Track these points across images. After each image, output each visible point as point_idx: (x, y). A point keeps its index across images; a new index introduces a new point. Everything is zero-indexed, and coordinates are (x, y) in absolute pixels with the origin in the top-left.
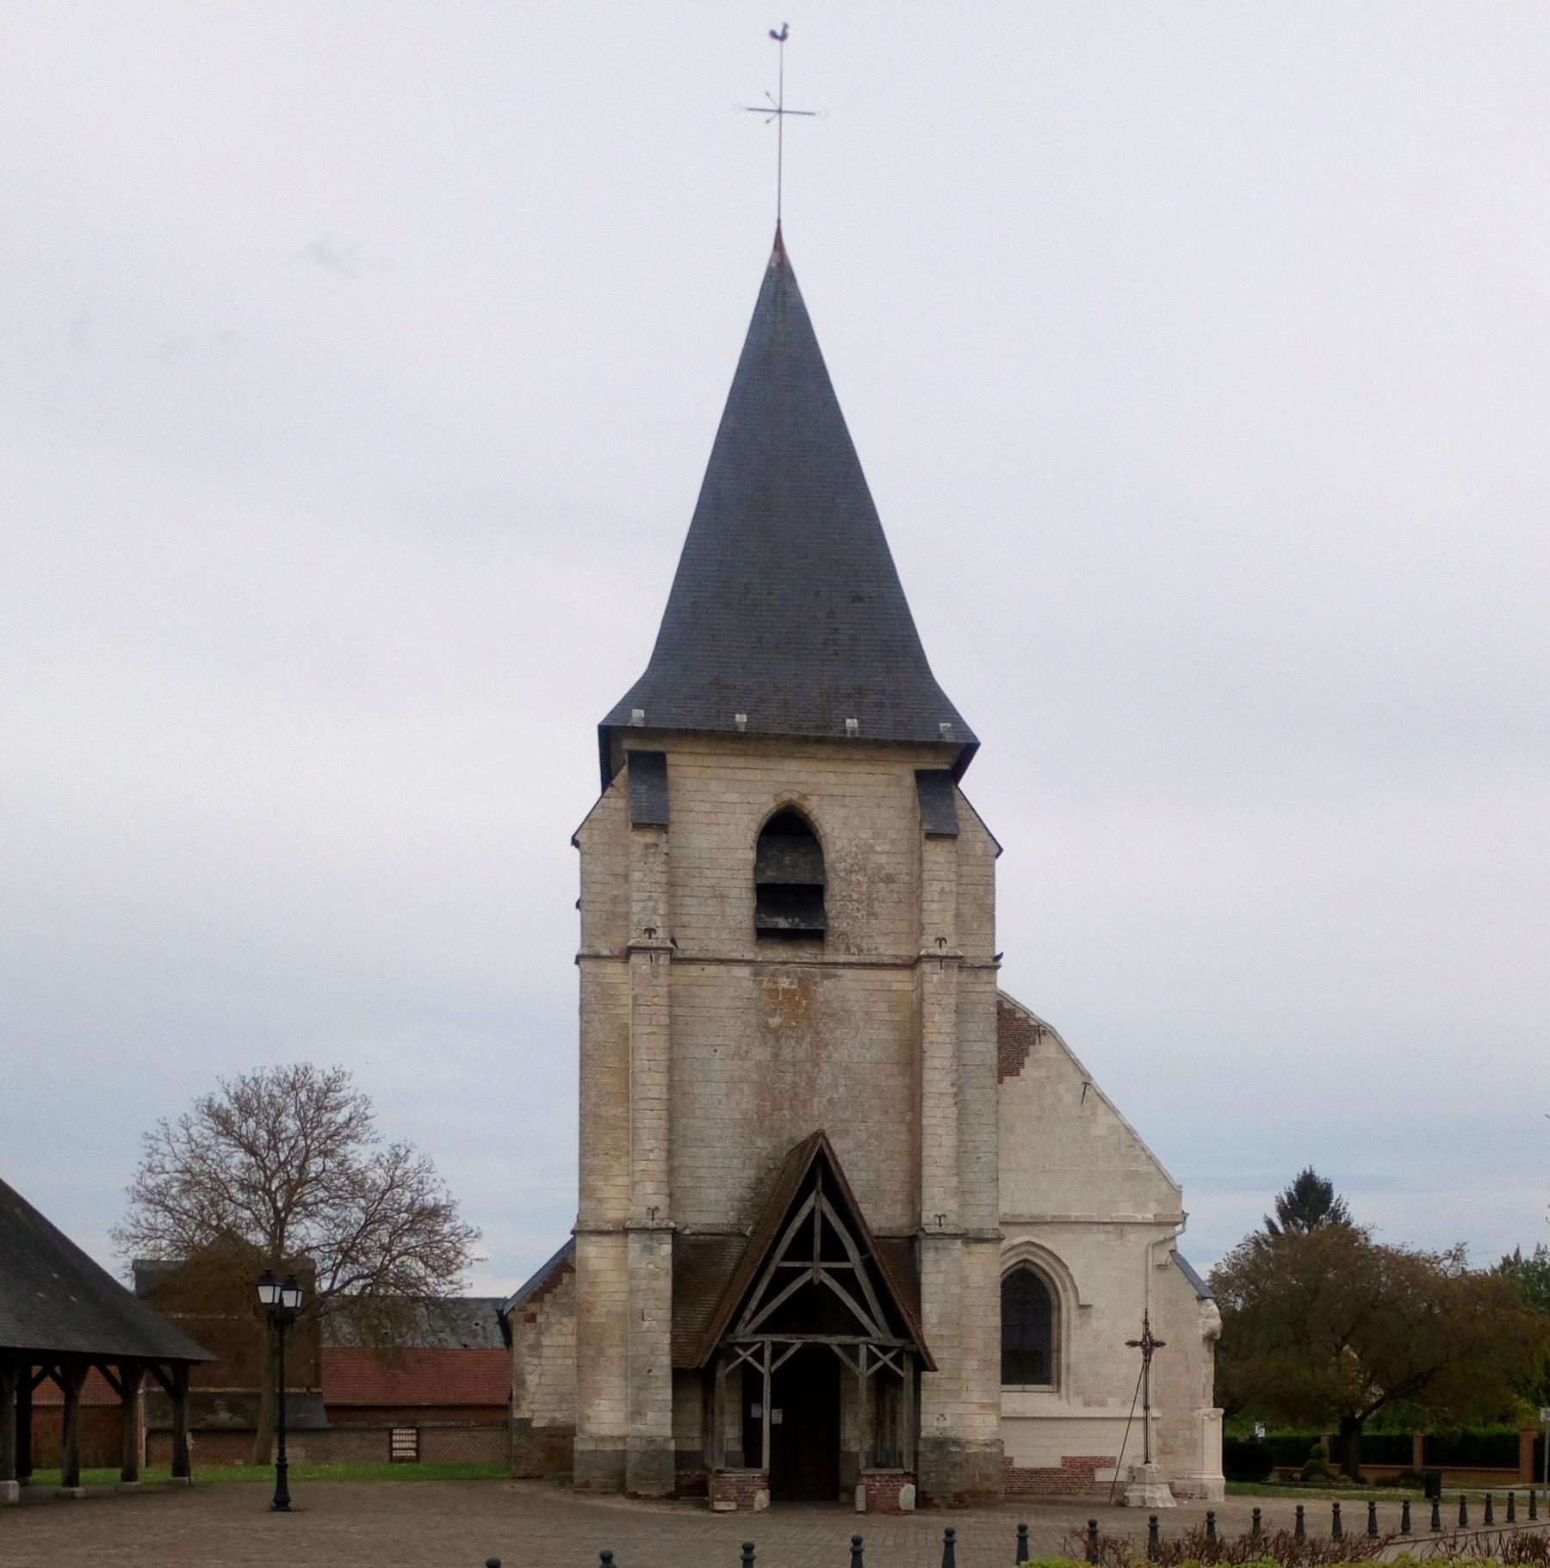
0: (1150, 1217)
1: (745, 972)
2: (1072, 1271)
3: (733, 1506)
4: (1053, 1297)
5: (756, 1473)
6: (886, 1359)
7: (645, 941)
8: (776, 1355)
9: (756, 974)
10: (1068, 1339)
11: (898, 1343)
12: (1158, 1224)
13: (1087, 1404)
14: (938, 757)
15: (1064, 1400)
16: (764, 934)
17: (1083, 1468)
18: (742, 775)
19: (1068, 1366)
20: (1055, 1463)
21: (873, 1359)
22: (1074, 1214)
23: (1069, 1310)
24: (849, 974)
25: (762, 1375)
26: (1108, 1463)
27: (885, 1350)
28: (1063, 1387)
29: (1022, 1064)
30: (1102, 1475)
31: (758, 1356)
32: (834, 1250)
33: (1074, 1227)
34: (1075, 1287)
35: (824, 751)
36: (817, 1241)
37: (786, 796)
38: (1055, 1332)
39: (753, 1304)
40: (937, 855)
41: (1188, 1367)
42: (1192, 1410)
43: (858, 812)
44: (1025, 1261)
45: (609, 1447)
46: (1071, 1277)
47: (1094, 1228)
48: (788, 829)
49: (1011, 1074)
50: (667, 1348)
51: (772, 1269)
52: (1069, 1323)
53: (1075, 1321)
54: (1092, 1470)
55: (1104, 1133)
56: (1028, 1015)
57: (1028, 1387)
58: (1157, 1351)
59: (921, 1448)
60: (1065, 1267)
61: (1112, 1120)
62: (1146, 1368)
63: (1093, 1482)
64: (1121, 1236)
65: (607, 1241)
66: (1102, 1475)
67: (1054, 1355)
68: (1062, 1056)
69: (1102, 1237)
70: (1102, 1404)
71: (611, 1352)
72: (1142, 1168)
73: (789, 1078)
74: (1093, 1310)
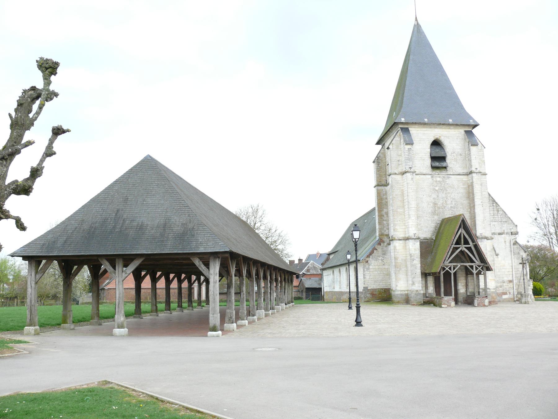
1: (430, 176)
3: (446, 306)
5: (451, 297)
6: (480, 268)
7: (409, 170)
8: (454, 269)
9: (432, 177)
11: (482, 264)
14: (469, 128)
16: (434, 168)
18: (426, 132)
21: (477, 268)
24: (453, 176)
25: (451, 273)
27: (479, 266)
31: (450, 269)
32: (466, 242)
35: (444, 127)
36: (462, 240)
37: (436, 137)
39: (448, 256)
40: (473, 149)
43: (453, 140)
45: (404, 293)
48: (436, 143)
50: (420, 268)
51: (452, 247)
59: (480, 291)
65: (401, 242)
71: (403, 269)
73: (441, 202)
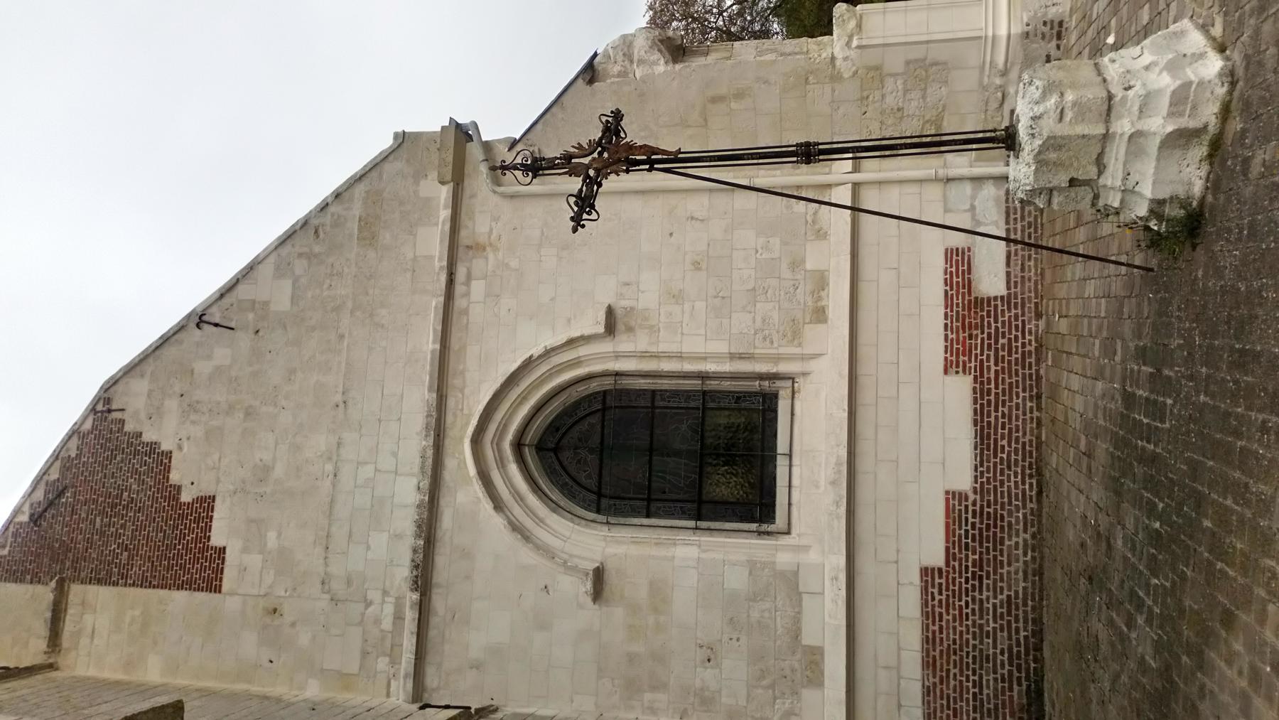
0: (444, 193)
2: (536, 351)
4: (594, 386)
10: (680, 357)
12: (458, 179)
13: (820, 315)
15: (812, 366)
17: (969, 316)
19: (733, 357)
20: (961, 388)
22: (430, 344)
23: (618, 356)
26: (959, 267)
28: (783, 368)
29: (153, 446)
30: (991, 278)
33: (454, 344)
34: (571, 343)
38: (665, 384)
41: (739, 95)
42: (836, 78)
44: (518, 446)
46: (548, 353)
47: (459, 303)
49: (168, 469)
52: (644, 355)
53: (642, 342)
54: (979, 303)
55: (287, 285)
56: (74, 432)
57: (782, 446)
58: (634, 133)
60: (528, 365)
61: (267, 269)
62: (673, 162)
63: (1007, 300)
64: (478, 248)
66: (991, 278)
67: (713, 385)
68: (149, 367)
69: (478, 287)
70: (821, 281)
72: (357, 209)
74: (621, 305)
